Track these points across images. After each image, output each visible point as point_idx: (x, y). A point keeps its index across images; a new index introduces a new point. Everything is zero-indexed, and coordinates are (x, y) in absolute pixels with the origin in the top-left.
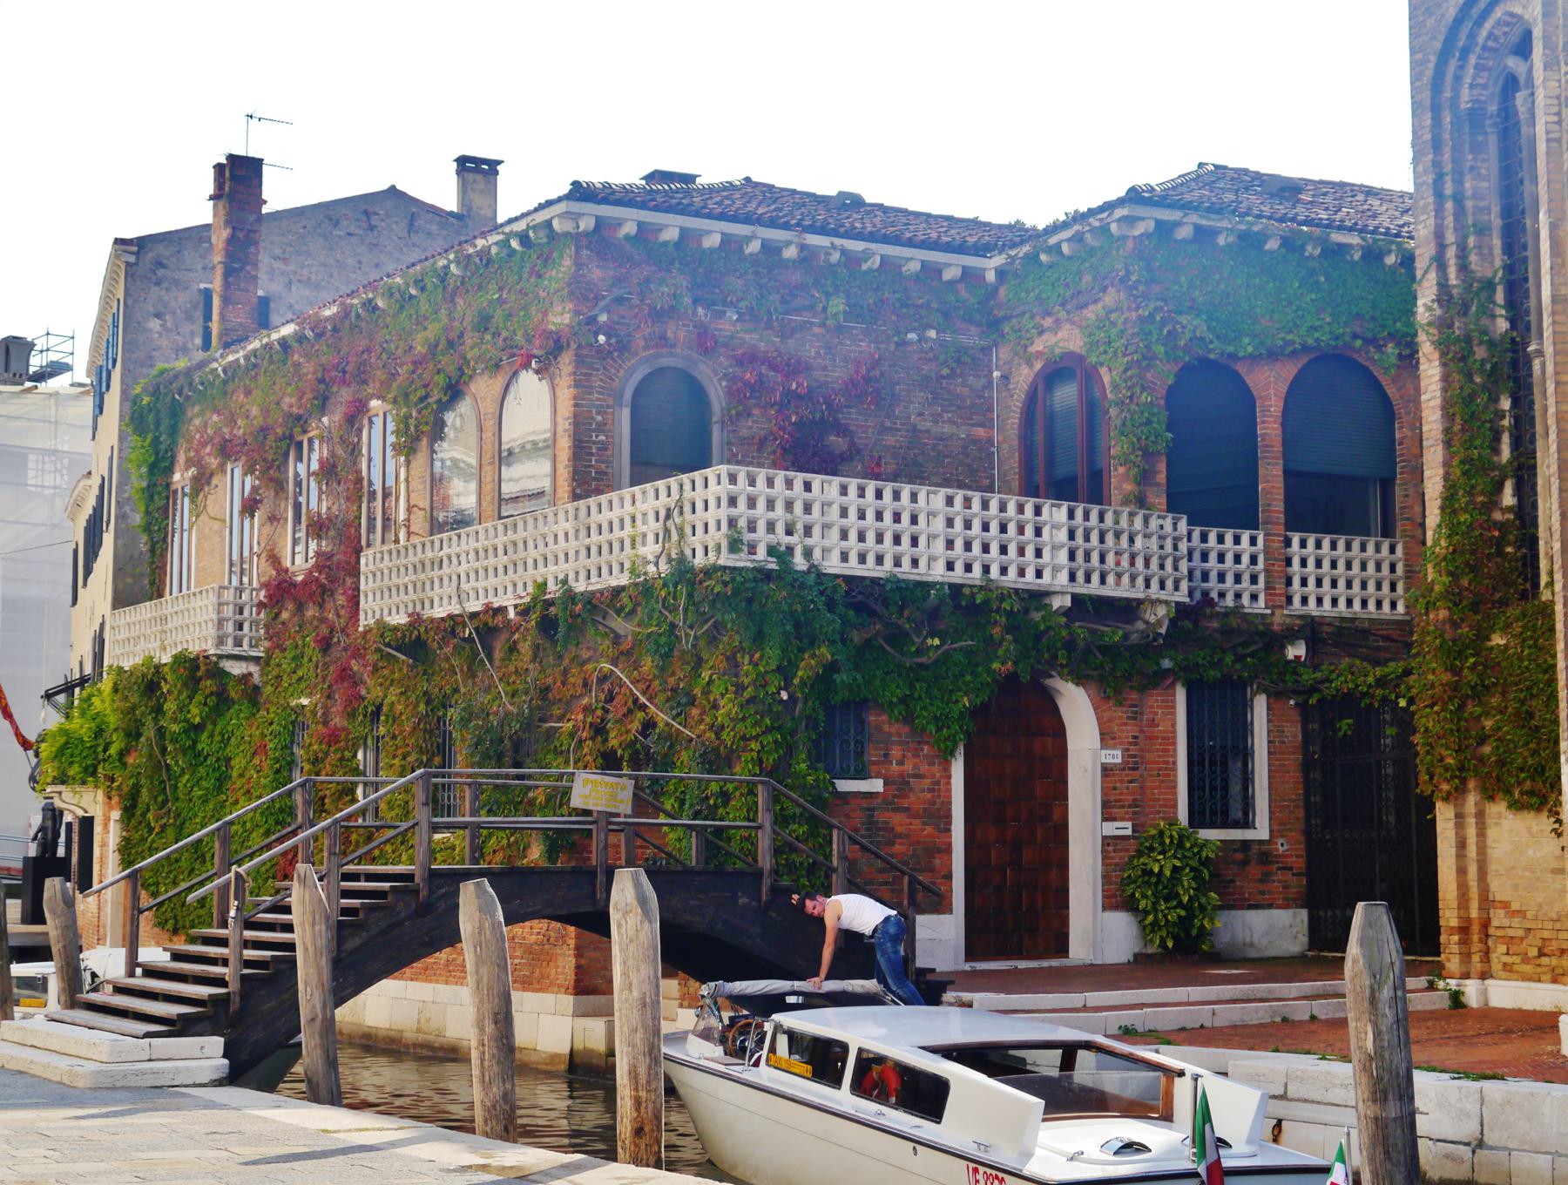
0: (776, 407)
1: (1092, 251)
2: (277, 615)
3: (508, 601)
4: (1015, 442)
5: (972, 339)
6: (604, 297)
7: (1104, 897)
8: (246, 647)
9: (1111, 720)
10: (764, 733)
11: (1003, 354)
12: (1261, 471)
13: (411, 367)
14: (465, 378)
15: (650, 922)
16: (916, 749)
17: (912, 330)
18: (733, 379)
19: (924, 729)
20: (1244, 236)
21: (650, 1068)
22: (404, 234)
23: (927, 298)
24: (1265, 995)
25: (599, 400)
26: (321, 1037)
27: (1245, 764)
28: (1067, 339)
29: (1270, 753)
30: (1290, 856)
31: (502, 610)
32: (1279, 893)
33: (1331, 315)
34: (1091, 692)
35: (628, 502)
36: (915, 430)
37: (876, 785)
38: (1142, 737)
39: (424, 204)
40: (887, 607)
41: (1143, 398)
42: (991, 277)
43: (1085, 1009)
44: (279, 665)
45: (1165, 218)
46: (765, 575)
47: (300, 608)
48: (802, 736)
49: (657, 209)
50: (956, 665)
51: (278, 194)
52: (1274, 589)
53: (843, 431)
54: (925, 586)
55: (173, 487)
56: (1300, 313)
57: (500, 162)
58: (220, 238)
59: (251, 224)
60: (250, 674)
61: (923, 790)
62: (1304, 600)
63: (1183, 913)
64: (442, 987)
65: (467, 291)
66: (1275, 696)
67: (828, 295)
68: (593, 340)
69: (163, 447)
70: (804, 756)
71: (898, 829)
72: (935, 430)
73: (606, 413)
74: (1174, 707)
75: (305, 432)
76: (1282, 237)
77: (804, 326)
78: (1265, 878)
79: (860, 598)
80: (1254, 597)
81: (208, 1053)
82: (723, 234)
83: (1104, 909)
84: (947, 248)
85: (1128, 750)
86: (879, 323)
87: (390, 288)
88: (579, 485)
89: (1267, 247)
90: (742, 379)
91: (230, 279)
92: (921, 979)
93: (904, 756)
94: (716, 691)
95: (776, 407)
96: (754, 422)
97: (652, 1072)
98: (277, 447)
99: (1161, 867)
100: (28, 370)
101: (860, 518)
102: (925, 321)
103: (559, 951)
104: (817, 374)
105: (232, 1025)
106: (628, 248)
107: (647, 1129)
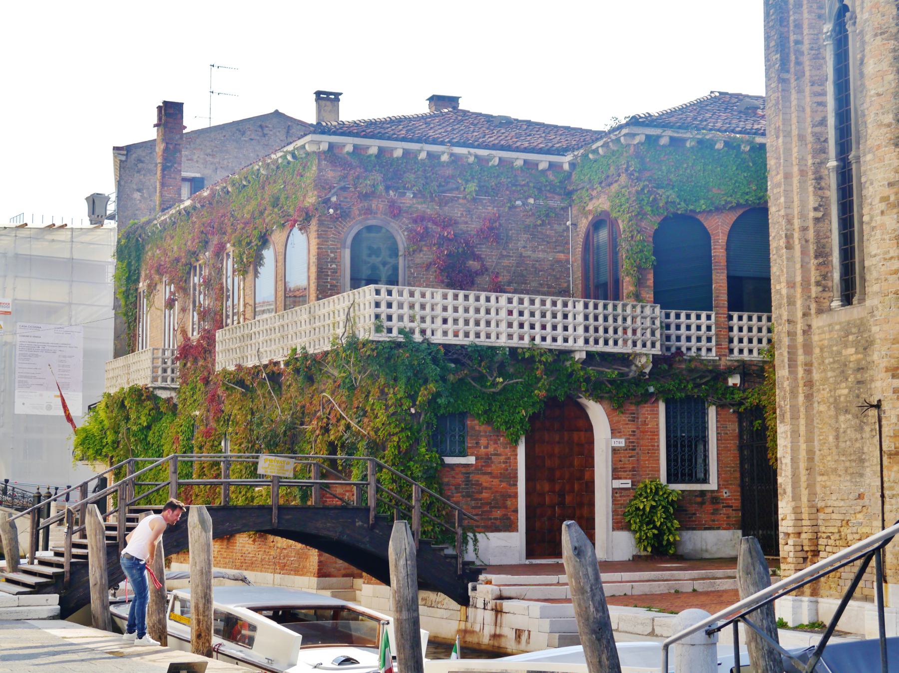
0: (437, 246)
1: (613, 153)
2: (185, 365)
3: (281, 358)
4: (580, 262)
5: (556, 203)
6: (334, 187)
7: (613, 523)
8: (169, 382)
9: (618, 422)
10: (400, 432)
11: (573, 212)
12: (714, 277)
13: (242, 226)
14: (269, 232)
15: (206, 532)
16: (496, 440)
17: (519, 199)
18: (410, 231)
19: (498, 429)
20: (700, 142)
21: (204, 604)
22: (283, 138)
23: (527, 180)
24: (669, 578)
25: (332, 245)
26: (99, 594)
27: (705, 446)
28: (601, 203)
29: (718, 440)
30: (731, 499)
31: (277, 364)
32: (724, 521)
33: (757, 185)
34: (606, 407)
35: (331, 304)
36: (521, 255)
37: (471, 460)
38: (638, 431)
39: (295, 120)
40: (471, 361)
41: (638, 237)
42: (566, 167)
43: (558, 584)
44: (185, 393)
45: (651, 133)
46: (399, 345)
47: (196, 360)
48: (424, 433)
49: (365, 136)
50: (518, 392)
51: (192, 122)
52: (721, 345)
53: (477, 258)
54: (493, 349)
55: (139, 291)
56: (737, 184)
57: (341, 94)
58: (160, 148)
59: (177, 141)
60: (172, 398)
61: (500, 463)
62: (741, 351)
63: (656, 532)
64: (259, 573)
65: (270, 183)
66: (721, 407)
67: (467, 181)
68: (326, 212)
69: (133, 268)
70: (424, 444)
71: (485, 484)
72: (534, 256)
73: (336, 252)
74: (658, 414)
75: (198, 261)
76: (724, 141)
77: (452, 199)
78: (715, 512)
79: (455, 356)
80: (709, 350)
81: (51, 602)
82: (403, 149)
83: (614, 529)
84: (540, 151)
85: (629, 439)
86: (499, 195)
87: (233, 181)
88: (320, 293)
89: (717, 147)
90: (415, 231)
91: (165, 172)
92: (466, 567)
93: (488, 444)
94: (377, 407)
95: (437, 246)
96: (424, 255)
97: (206, 607)
98: (183, 269)
99: (645, 506)
100: (106, 213)
101: (519, 304)
102: (526, 194)
103: (311, 553)
104: (462, 227)
105: (65, 588)
106: (349, 159)
107: (203, 635)
